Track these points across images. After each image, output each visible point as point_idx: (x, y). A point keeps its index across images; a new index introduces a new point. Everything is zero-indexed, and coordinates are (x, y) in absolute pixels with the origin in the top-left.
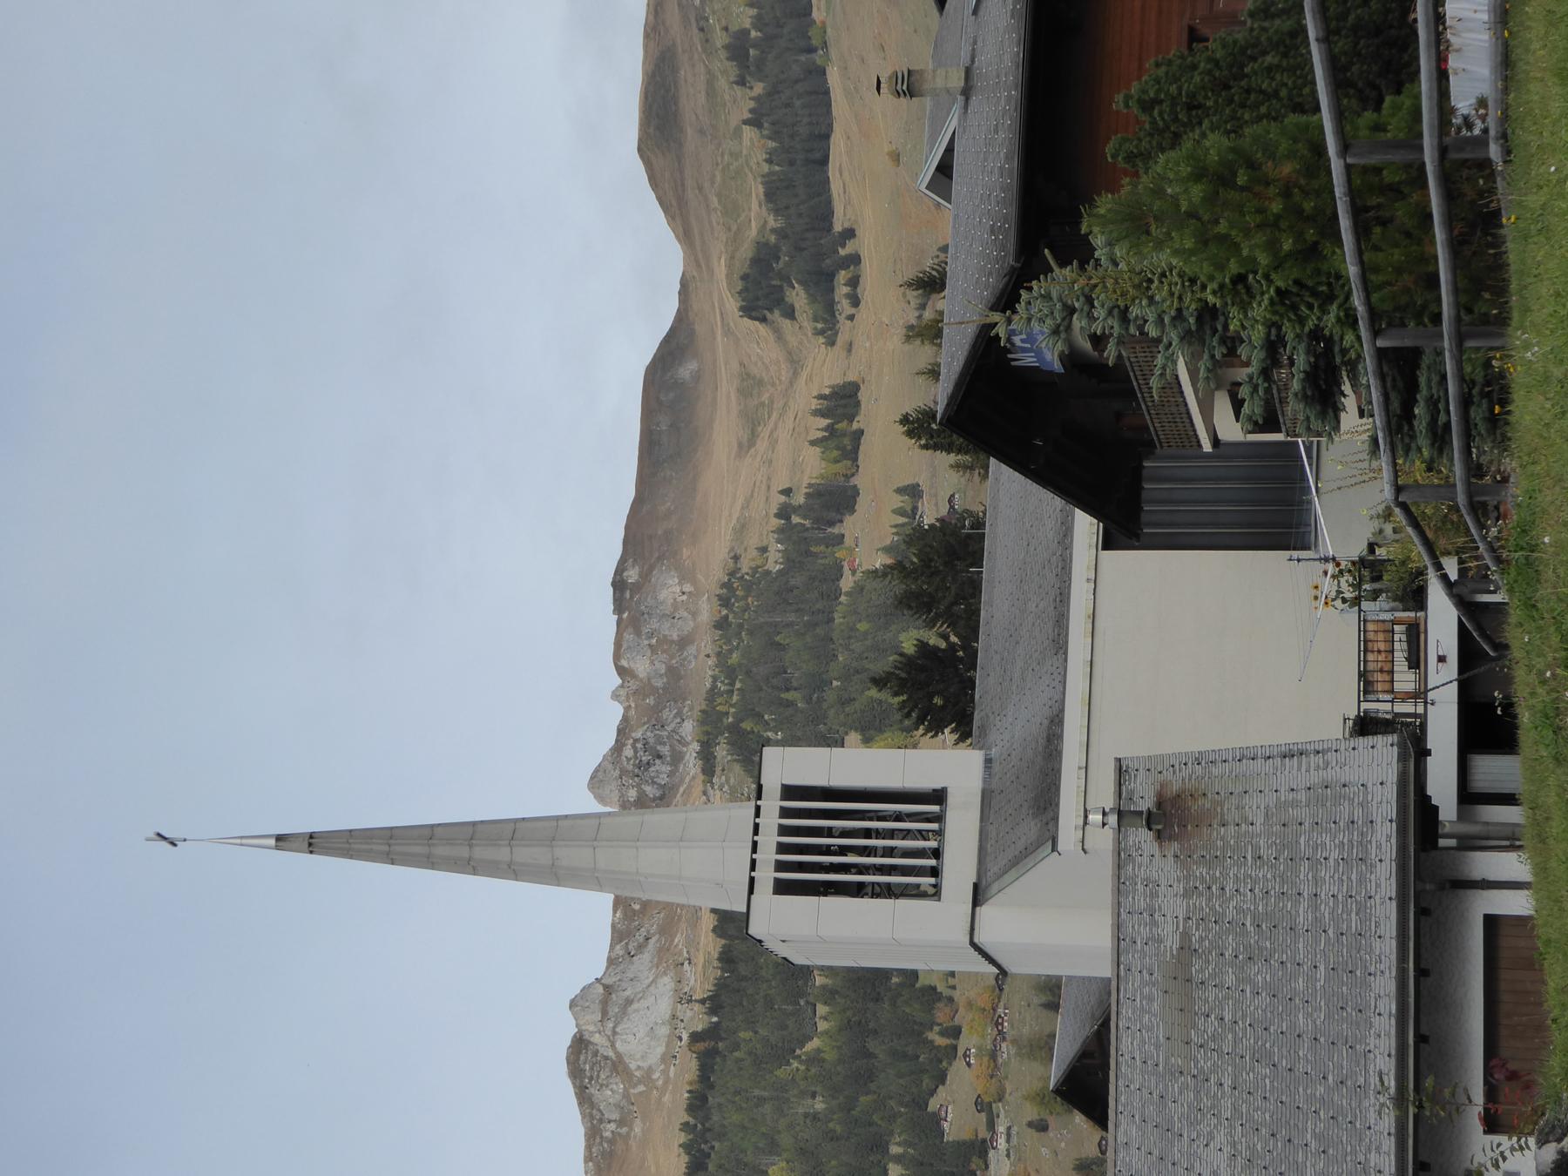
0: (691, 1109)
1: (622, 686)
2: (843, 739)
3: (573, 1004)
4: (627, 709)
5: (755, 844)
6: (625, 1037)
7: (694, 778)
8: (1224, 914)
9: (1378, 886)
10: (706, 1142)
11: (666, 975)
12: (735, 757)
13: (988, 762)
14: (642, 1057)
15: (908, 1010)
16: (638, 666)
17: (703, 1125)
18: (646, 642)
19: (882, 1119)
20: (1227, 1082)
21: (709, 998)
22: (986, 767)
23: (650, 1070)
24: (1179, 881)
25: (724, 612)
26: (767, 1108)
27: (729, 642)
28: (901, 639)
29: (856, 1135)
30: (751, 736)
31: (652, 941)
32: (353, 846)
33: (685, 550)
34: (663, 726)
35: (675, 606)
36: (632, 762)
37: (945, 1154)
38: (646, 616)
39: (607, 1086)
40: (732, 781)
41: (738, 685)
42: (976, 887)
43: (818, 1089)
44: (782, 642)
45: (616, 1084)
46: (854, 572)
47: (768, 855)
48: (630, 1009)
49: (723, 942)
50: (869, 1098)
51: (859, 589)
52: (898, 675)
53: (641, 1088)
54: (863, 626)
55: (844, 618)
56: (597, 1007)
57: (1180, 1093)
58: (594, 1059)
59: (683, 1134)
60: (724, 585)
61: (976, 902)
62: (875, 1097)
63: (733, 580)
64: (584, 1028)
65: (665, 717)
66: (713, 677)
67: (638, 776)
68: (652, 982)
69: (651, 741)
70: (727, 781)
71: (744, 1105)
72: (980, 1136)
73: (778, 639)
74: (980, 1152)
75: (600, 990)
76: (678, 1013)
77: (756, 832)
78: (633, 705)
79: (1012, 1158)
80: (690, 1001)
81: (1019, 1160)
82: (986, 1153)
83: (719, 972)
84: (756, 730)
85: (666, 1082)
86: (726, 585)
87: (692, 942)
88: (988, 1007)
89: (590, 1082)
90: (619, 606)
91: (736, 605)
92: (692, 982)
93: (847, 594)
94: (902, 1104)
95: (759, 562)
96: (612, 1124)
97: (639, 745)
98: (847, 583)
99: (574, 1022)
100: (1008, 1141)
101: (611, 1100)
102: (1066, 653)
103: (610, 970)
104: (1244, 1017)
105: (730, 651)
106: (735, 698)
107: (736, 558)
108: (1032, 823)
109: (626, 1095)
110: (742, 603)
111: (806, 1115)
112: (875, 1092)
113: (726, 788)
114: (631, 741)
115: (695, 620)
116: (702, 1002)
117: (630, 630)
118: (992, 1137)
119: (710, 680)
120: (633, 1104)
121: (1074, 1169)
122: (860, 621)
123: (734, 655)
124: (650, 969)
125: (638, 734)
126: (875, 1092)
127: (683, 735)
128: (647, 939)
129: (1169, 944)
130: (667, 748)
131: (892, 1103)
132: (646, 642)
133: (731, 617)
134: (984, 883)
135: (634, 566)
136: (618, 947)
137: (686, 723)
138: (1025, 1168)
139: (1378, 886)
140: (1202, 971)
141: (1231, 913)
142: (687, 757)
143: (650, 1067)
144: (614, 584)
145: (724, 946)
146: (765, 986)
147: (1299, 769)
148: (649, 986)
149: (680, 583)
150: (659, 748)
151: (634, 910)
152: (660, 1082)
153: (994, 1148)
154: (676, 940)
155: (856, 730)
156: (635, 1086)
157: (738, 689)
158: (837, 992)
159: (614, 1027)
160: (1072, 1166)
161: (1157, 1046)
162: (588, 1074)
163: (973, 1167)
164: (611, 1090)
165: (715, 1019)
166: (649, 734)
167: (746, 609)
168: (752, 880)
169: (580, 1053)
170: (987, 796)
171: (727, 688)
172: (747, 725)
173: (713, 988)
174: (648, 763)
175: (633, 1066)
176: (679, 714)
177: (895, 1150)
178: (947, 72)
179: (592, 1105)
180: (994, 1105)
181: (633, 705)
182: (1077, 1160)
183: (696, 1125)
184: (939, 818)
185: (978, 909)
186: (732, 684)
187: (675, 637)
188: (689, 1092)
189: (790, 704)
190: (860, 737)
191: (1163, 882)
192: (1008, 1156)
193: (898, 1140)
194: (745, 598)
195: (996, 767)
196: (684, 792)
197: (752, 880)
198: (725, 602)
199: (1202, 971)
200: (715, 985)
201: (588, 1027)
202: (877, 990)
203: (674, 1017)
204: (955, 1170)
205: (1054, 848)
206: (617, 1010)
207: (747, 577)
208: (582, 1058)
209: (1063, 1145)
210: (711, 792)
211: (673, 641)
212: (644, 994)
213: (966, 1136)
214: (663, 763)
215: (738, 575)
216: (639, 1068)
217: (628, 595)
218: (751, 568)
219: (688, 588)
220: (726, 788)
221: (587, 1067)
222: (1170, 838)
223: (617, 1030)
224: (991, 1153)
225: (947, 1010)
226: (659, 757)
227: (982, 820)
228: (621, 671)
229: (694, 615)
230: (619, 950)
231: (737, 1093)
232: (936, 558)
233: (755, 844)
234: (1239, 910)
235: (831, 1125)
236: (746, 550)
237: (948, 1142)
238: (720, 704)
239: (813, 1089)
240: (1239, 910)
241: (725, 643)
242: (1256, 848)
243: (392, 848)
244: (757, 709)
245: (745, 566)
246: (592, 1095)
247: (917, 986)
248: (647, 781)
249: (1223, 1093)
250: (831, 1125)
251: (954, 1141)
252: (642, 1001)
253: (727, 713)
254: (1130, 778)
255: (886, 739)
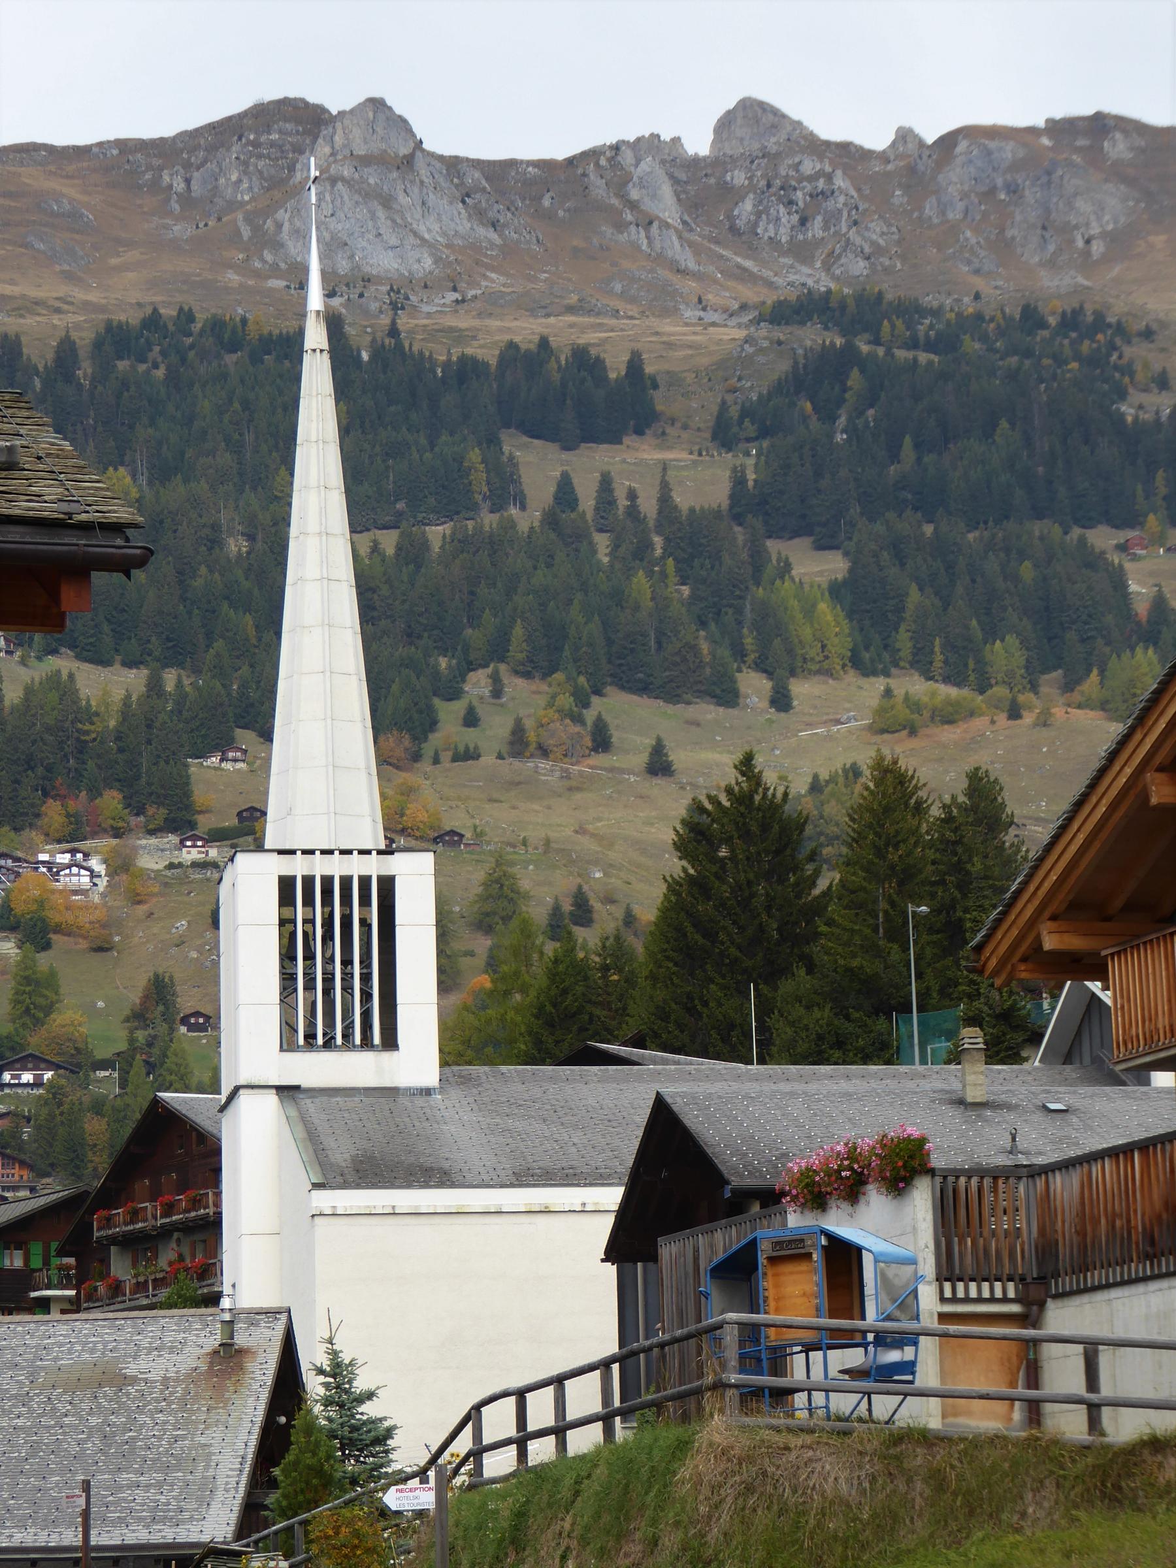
0: (216, 325)
1: (921, 143)
2: (837, 548)
3: (377, 105)
4: (883, 157)
5: (331, 852)
6: (328, 197)
7: (770, 285)
8: (142, 1413)
9: (134, 1531)
10: (163, 353)
11: (436, 262)
12: (802, 361)
13: (428, 1092)
14: (297, 231)
15: (395, 688)
16: (958, 170)
17: (192, 347)
18: (999, 182)
19: (218, 655)
20: (19, 1422)
21: (399, 346)
22: (422, 1090)
23: (277, 246)
24: (177, 1372)
25: (1052, 321)
26: (225, 459)
27: (1001, 332)
28: (1008, 637)
29: (190, 613)
30: (837, 388)
31: (493, 236)
32: (314, 400)
33: (1163, 238)
34: (855, 223)
35: (1067, 230)
36: (792, 173)
37: (167, 762)
38: (1044, 179)
39: (245, 172)
40: (761, 359)
41: (923, 357)
42: (297, 1088)
43: (259, 545)
44: (998, 431)
45: (251, 188)
46: (1123, 548)
47: (320, 867)
48: (375, 205)
49: (493, 362)
50: (252, 632)
51: (1092, 560)
52: (756, 792)
53: (246, 232)
54: (1027, 571)
55: (1041, 538)
56: (376, 146)
57: (17, 1381)
58: (288, 147)
59: (175, 313)
60: (1099, 317)
61: (280, 1089)
62: (254, 641)
63: (1109, 332)
64: (338, 125)
65: (872, 225)
66: (941, 307)
67: (769, 186)
68: (422, 239)
69: (830, 204)
70: (761, 350)
71: (226, 420)
72: (200, 819)
73: (1004, 424)
74: (174, 820)
75: (404, 151)
76: (373, 288)
77: (343, 852)
78: (890, 167)
79: (168, 873)
80: (395, 307)
81: (166, 884)
82: (174, 831)
83: (443, 358)
84: (847, 396)
85: (257, 274)
86: (1100, 322)
87: (493, 303)
88: (407, 821)
89: (249, 143)
90: (1061, 129)
91: (1066, 342)
92: (426, 308)
93: (1082, 540)
94: (244, 686)
95: (1140, 376)
96: (183, 185)
97: (821, 184)
98: (1103, 538)
99: (348, 108)
100: (195, 865)
101: (222, 181)
102: (512, 1186)
103: (438, 165)
104: (64, 1433)
105: (984, 338)
106: (901, 354)
107: (1148, 334)
108: (347, 1156)
109: (233, 205)
110: (1067, 351)
111: (215, 527)
112: (260, 640)
113: (749, 349)
114: (828, 169)
115: (1041, 264)
116: (394, 332)
117: (1021, 153)
118: (201, 839)
119: (935, 304)
120: (219, 219)
121: (156, 976)
122: (1035, 566)
123: (977, 346)
124: (444, 234)
125: (840, 181)
126: (260, 640)
127: (843, 260)
128: (494, 225)
129: (131, 1366)
130: (820, 234)
131: (245, 670)
132: (999, 182)
133: (1045, 333)
134: (301, 1096)
135: (1132, 149)
136: (477, 175)
137: (862, 264)
138: (152, 895)
139: (134, 1531)
140: (105, 1396)
141: (142, 1419)
142: (806, 270)
143: (282, 245)
144: (1099, 117)
145: (486, 365)
146: (423, 441)
147: (231, 1470)
148: (415, 234)
149: (1104, 235)
150: (819, 218)
151: (541, 197)
152: (258, 264)
153: (182, 842)
154: (493, 276)
155: (851, 571)
156: (248, 220)
157: (915, 360)
158: (419, 567)
159: (343, 179)
160: (161, 971)
161: (56, 1359)
162: (263, 139)
163: (151, 810)
164: (240, 181)
165: (365, 356)
166: (842, 199)
167: (1060, 361)
168: (292, 852)
169: (298, 122)
170: (392, 1092)
171: (921, 335)
172: (855, 379)
173: (415, 348)
174: (791, 202)
175: (281, 215)
176: (878, 250)
177: (170, 678)
178: (981, 1085)
179: (212, 149)
180: (250, 839)
181: (890, 167)
182: (171, 978)
183: (190, 335)
184: (367, 1043)
185: (274, 1091)
186: (930, 347)
187: (1009, 233)
188: (244, 321)
189: (894, 455)
190: (840, 577)
191: (179, 1358)
192: (171, 866)
193: (186, 682)
194: (1077, 357)
195: (420, 1101)
196: (745, 270)
197: (292, 852)
198: (1071, 321)
199: (105, 1396)
200: (421, 353)
201: (339, 131)
202: (426, 635)
203: (367, 280)
204: (144, 780)
205: (317, 1186)
206: (372, 181)
207: (1115, 357)
208: (289, 126)
209: (194, 955)
210: (746, 318)
211: (1002, 231)
212: (402, 226)
213: (200, 795)
214: (792, 228)
215: (1118, 341)
216: (279, 226)
217: (1081, 142)
218: (1130, 364)
219: (1097, 248)
220: (749, 349)
221: (275, 136)
222: (211, 1364)
223: (340, 185)
224: (173, 839)
225: (399, 752)
226: (803, 221)
227: (367, 1089)
228: (948, 141)
229: (1051, 264)
230: (473, 177)
231: (246, 405)
232: (900, 852)
233: (331, 852)
234: (142, 1426)
235: (203, 570)
236: (1163, 350)
237: (187, 766)
238: (893, 326)
239: (260, 536)
240: (142, 1426)
241: (999, 326)
242: (184, 1437)
243: (314, 445)
244: (883, 394)
245: (1135, 351)
246: (228, 149)
247: (437, 702)
248: (760, 202)
249: (13, 1419)
250: (203, 570)
251: (188, 777)
252: (389, 222)
253: (877, 342)
254: (269, 1322)
255: (838, 624)
